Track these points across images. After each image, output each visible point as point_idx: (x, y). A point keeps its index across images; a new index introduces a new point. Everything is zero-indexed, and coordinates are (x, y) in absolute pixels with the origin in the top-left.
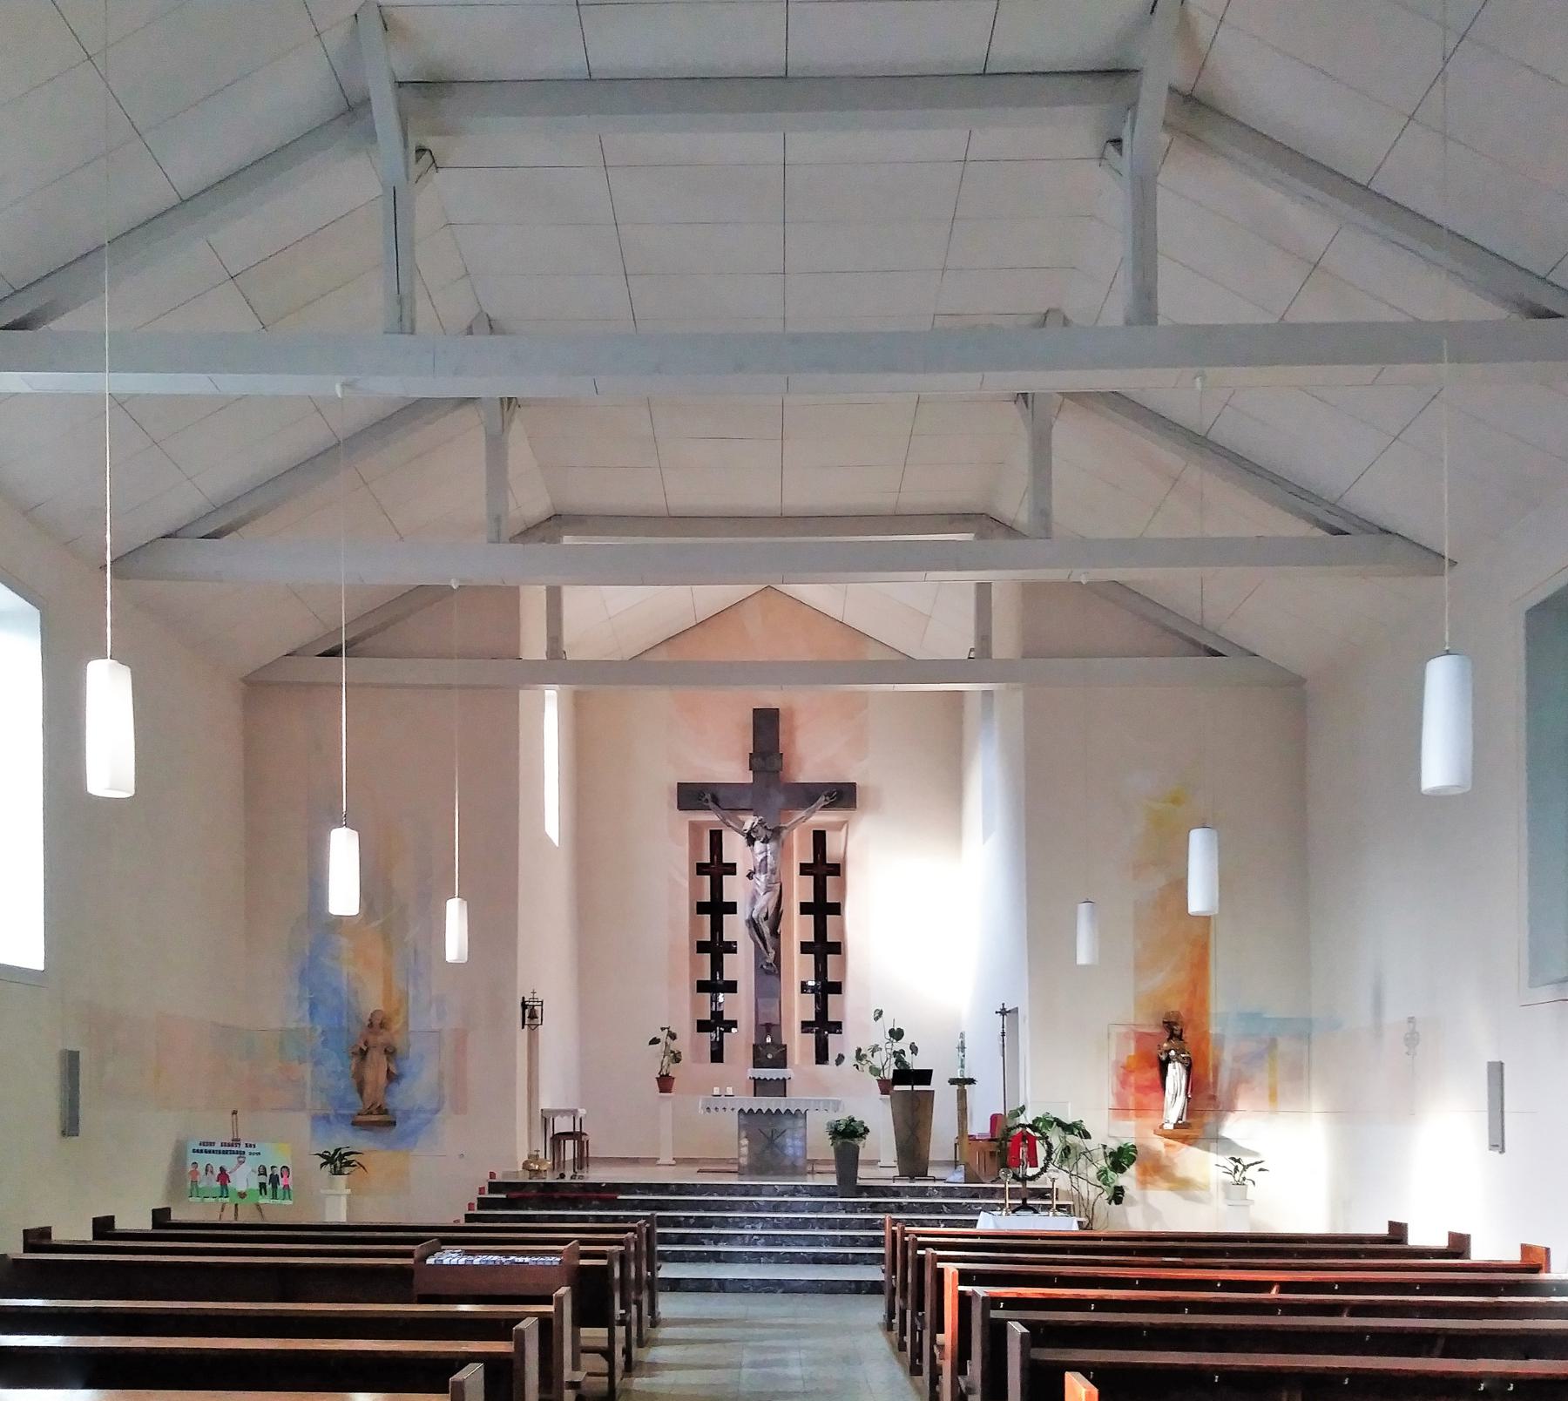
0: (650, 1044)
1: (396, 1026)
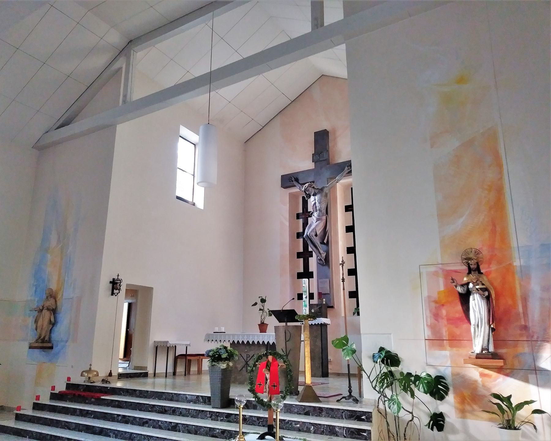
0: (252, 306)
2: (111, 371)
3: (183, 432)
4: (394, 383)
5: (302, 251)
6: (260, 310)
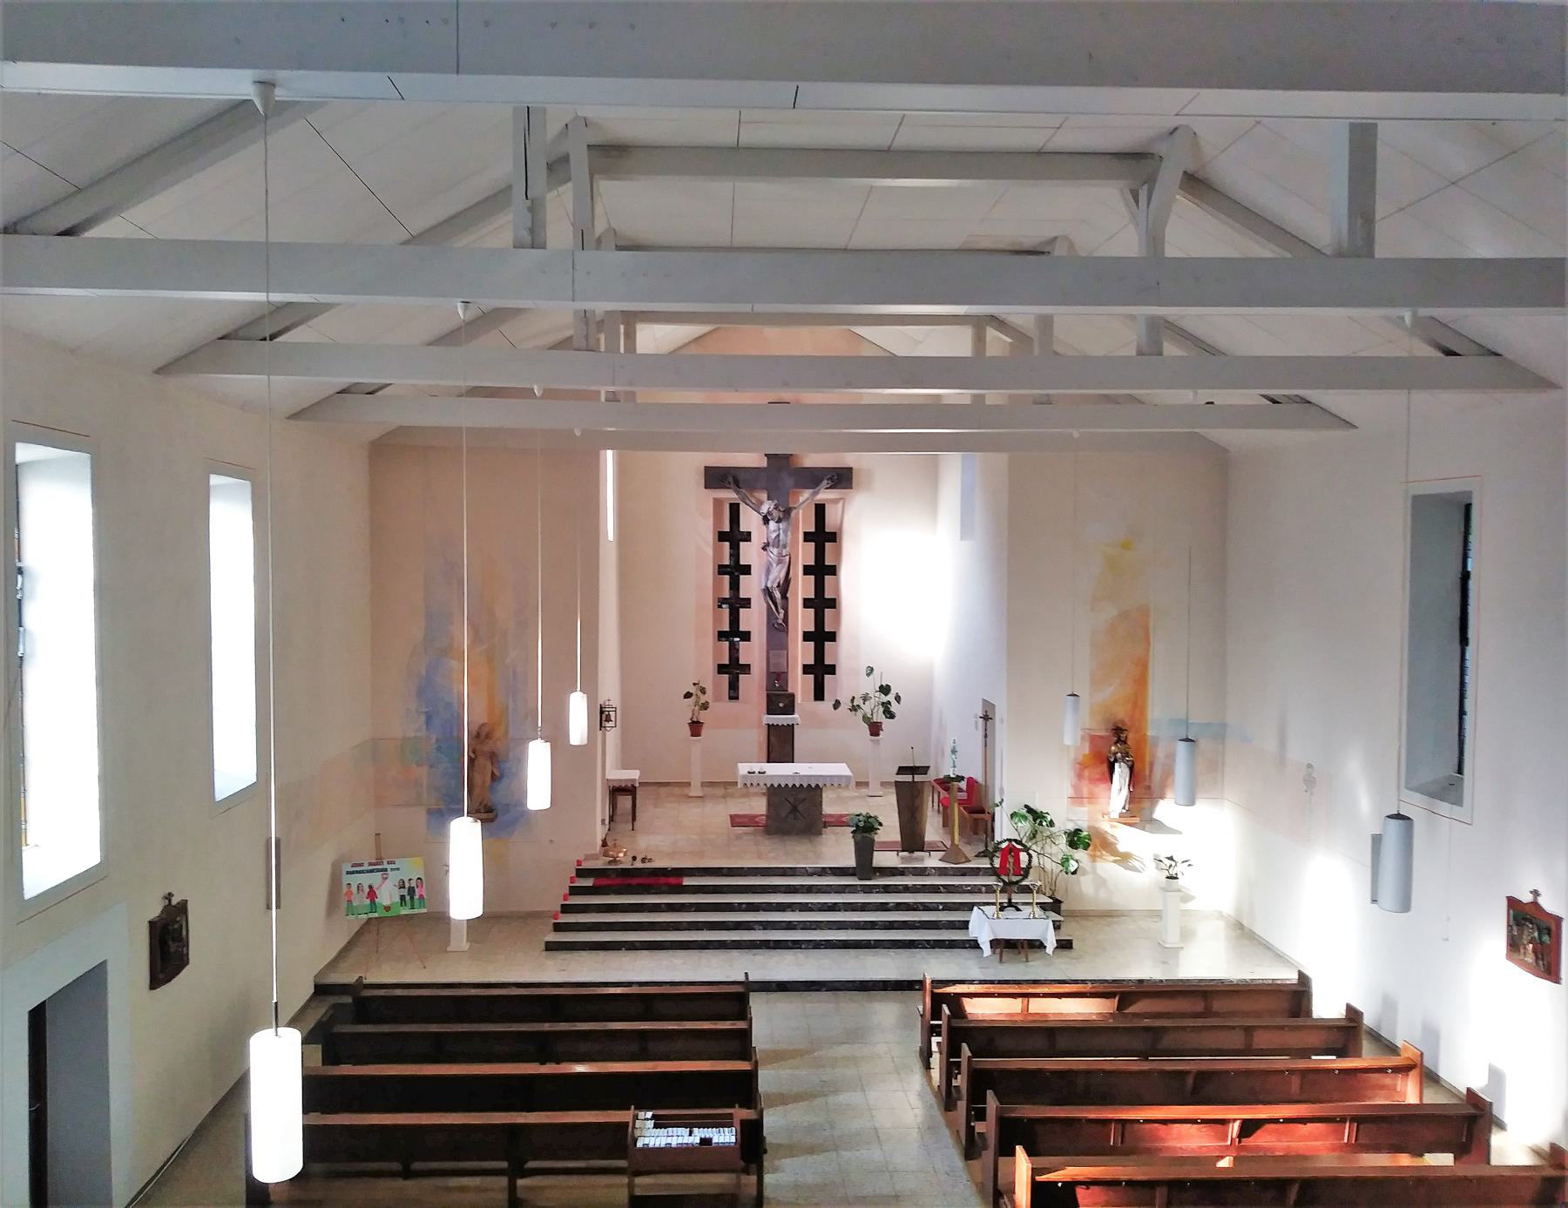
1: (498, 733)
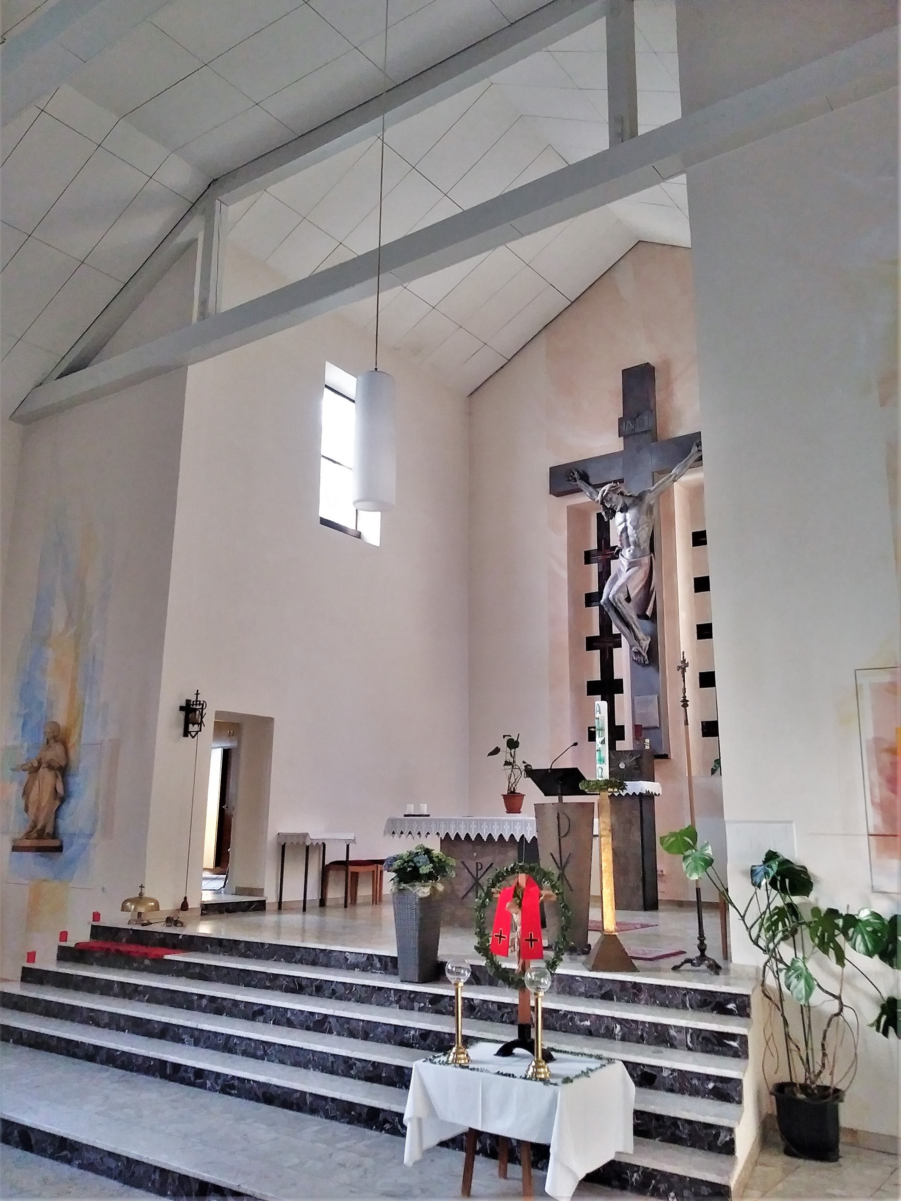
0: (488, 755)
2: (185, 898)
3: (339, 1034)
4: (799, 931)
5: (599, 635)
6: (507, 763)
